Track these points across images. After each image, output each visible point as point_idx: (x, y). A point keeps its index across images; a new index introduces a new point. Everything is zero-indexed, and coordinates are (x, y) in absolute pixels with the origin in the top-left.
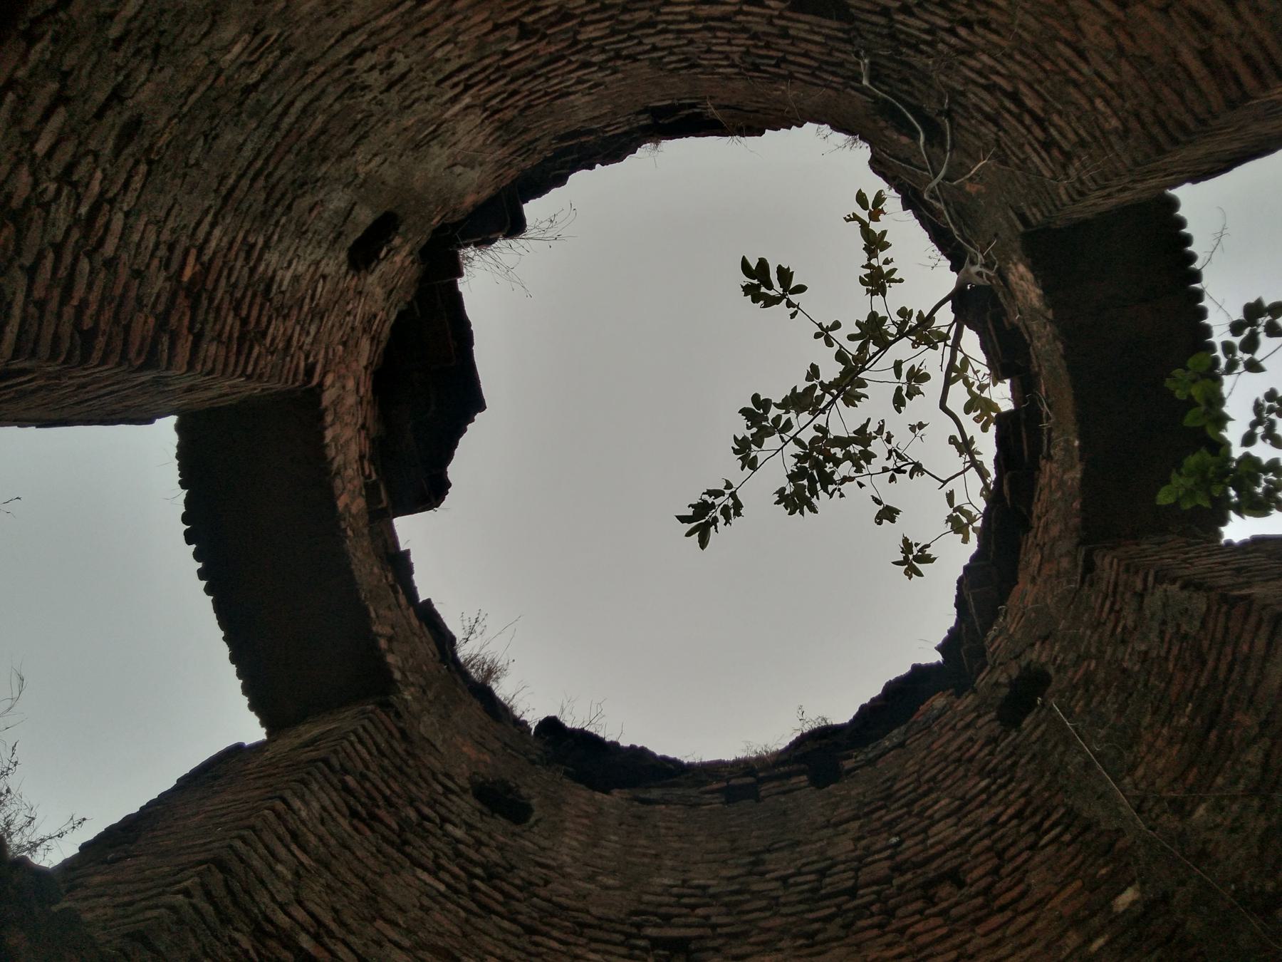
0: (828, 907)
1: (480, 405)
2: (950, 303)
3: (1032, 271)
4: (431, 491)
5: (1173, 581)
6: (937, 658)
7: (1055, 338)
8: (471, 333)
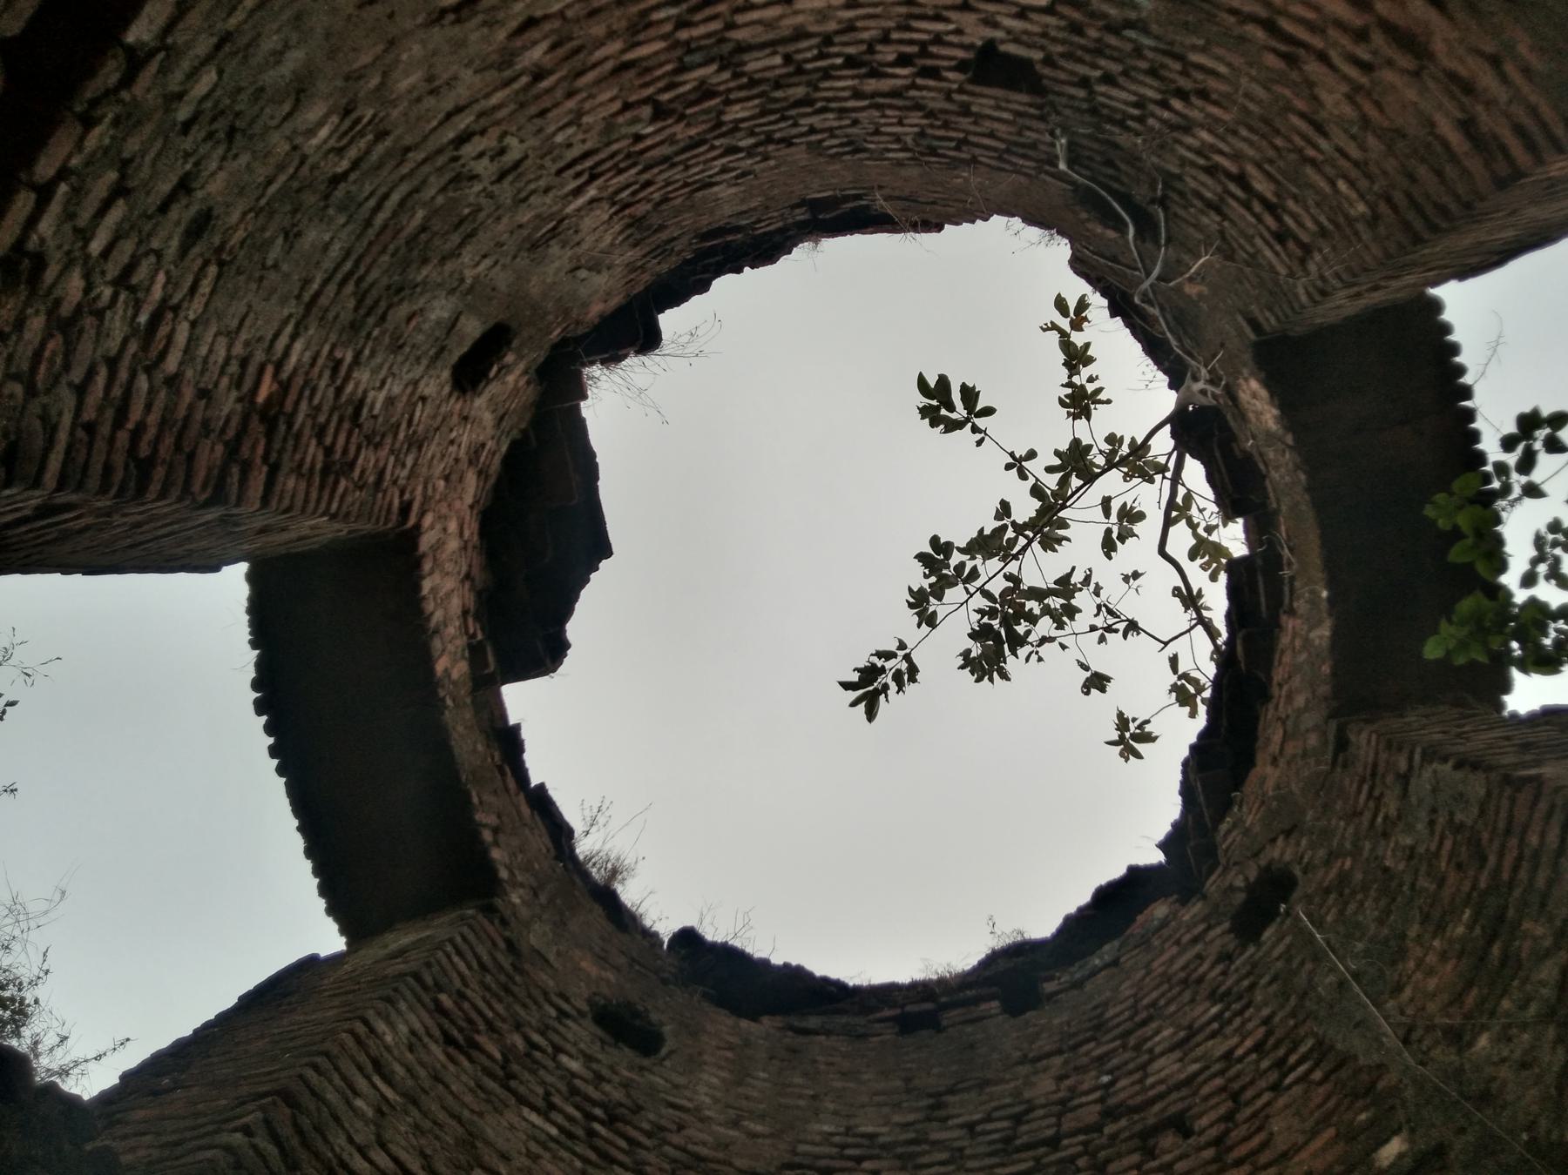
0: (1025, 1160)
2: (1168, 428)
4: (542, 651)
5: (1445, 760)
6: (1158, 857)
7: (1297, 468)
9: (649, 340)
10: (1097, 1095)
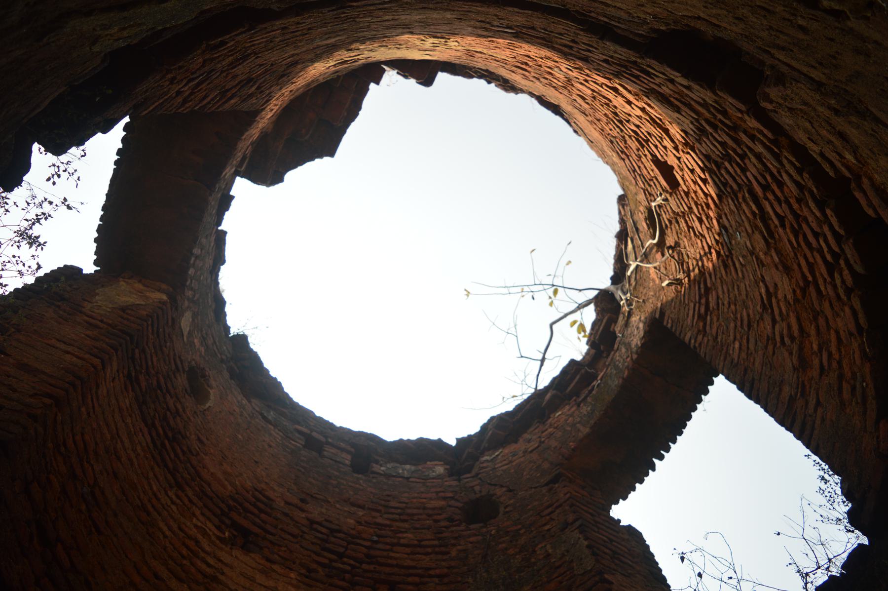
0: (325, 557)
1: (329, 149)
2: (596, 292)
3: (645, 333)
5: (586, 539)
7: (627, 367)
8: (357, 114)
9: (427, 80)
10: (368, 544)
